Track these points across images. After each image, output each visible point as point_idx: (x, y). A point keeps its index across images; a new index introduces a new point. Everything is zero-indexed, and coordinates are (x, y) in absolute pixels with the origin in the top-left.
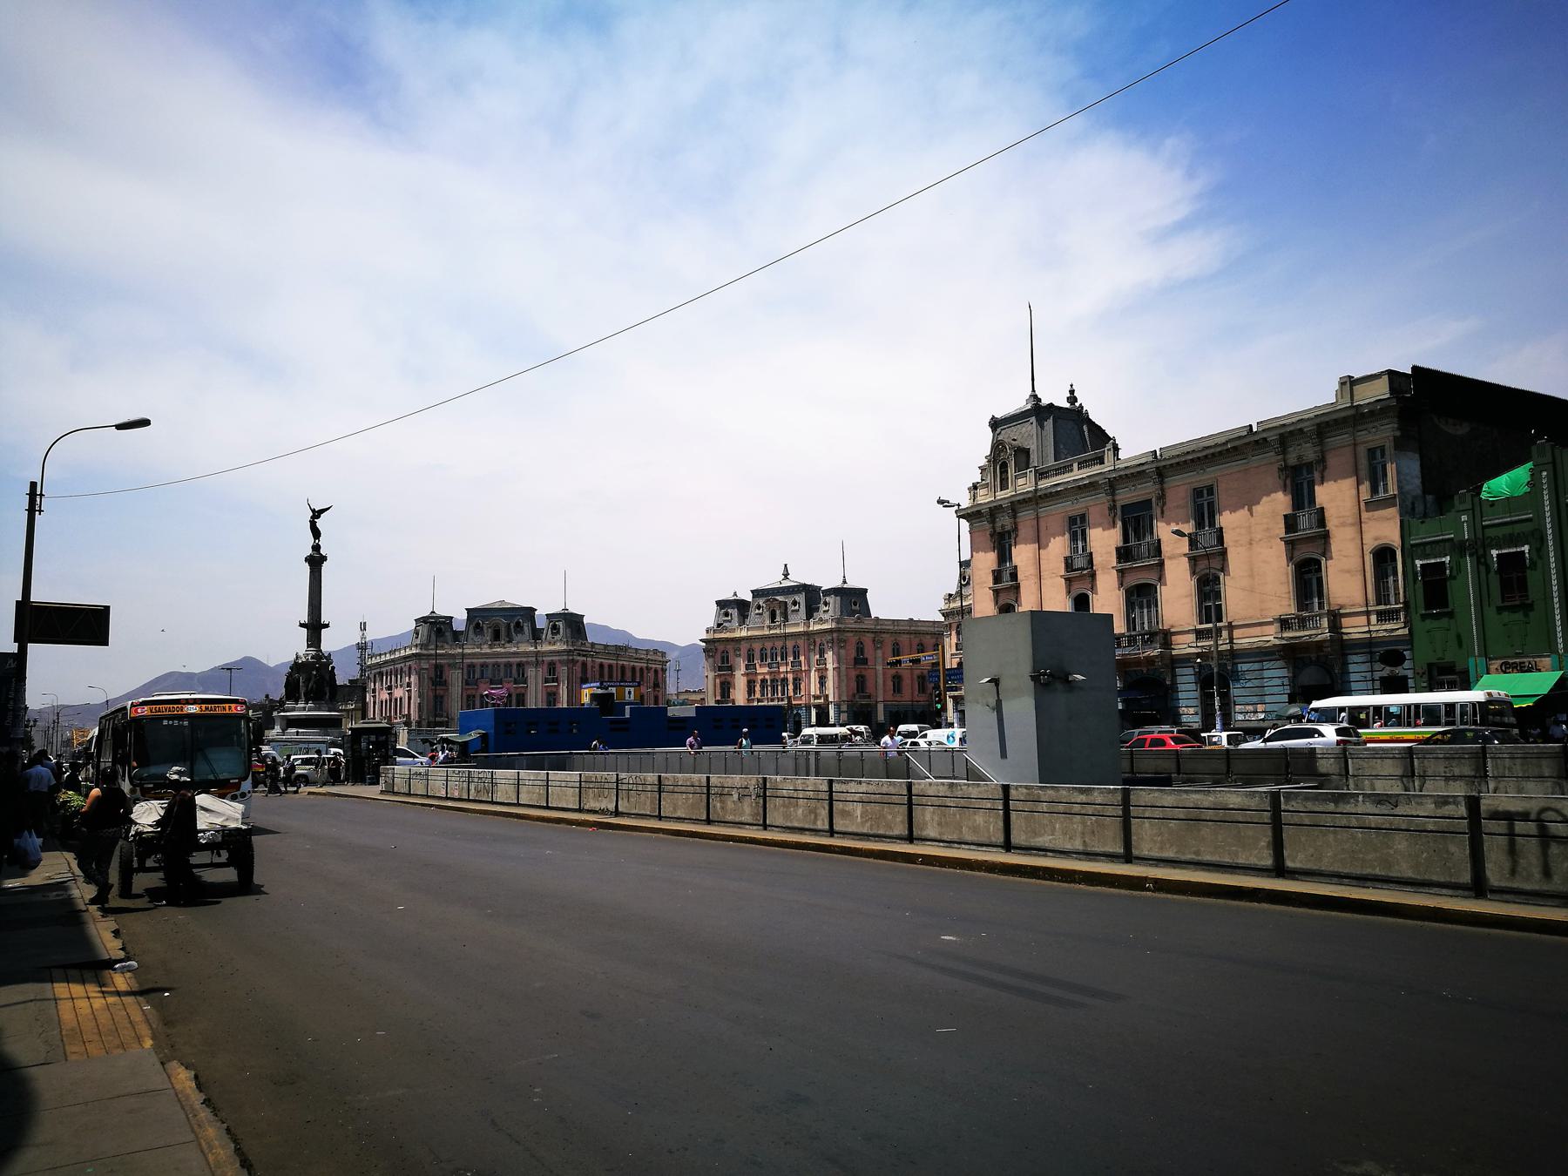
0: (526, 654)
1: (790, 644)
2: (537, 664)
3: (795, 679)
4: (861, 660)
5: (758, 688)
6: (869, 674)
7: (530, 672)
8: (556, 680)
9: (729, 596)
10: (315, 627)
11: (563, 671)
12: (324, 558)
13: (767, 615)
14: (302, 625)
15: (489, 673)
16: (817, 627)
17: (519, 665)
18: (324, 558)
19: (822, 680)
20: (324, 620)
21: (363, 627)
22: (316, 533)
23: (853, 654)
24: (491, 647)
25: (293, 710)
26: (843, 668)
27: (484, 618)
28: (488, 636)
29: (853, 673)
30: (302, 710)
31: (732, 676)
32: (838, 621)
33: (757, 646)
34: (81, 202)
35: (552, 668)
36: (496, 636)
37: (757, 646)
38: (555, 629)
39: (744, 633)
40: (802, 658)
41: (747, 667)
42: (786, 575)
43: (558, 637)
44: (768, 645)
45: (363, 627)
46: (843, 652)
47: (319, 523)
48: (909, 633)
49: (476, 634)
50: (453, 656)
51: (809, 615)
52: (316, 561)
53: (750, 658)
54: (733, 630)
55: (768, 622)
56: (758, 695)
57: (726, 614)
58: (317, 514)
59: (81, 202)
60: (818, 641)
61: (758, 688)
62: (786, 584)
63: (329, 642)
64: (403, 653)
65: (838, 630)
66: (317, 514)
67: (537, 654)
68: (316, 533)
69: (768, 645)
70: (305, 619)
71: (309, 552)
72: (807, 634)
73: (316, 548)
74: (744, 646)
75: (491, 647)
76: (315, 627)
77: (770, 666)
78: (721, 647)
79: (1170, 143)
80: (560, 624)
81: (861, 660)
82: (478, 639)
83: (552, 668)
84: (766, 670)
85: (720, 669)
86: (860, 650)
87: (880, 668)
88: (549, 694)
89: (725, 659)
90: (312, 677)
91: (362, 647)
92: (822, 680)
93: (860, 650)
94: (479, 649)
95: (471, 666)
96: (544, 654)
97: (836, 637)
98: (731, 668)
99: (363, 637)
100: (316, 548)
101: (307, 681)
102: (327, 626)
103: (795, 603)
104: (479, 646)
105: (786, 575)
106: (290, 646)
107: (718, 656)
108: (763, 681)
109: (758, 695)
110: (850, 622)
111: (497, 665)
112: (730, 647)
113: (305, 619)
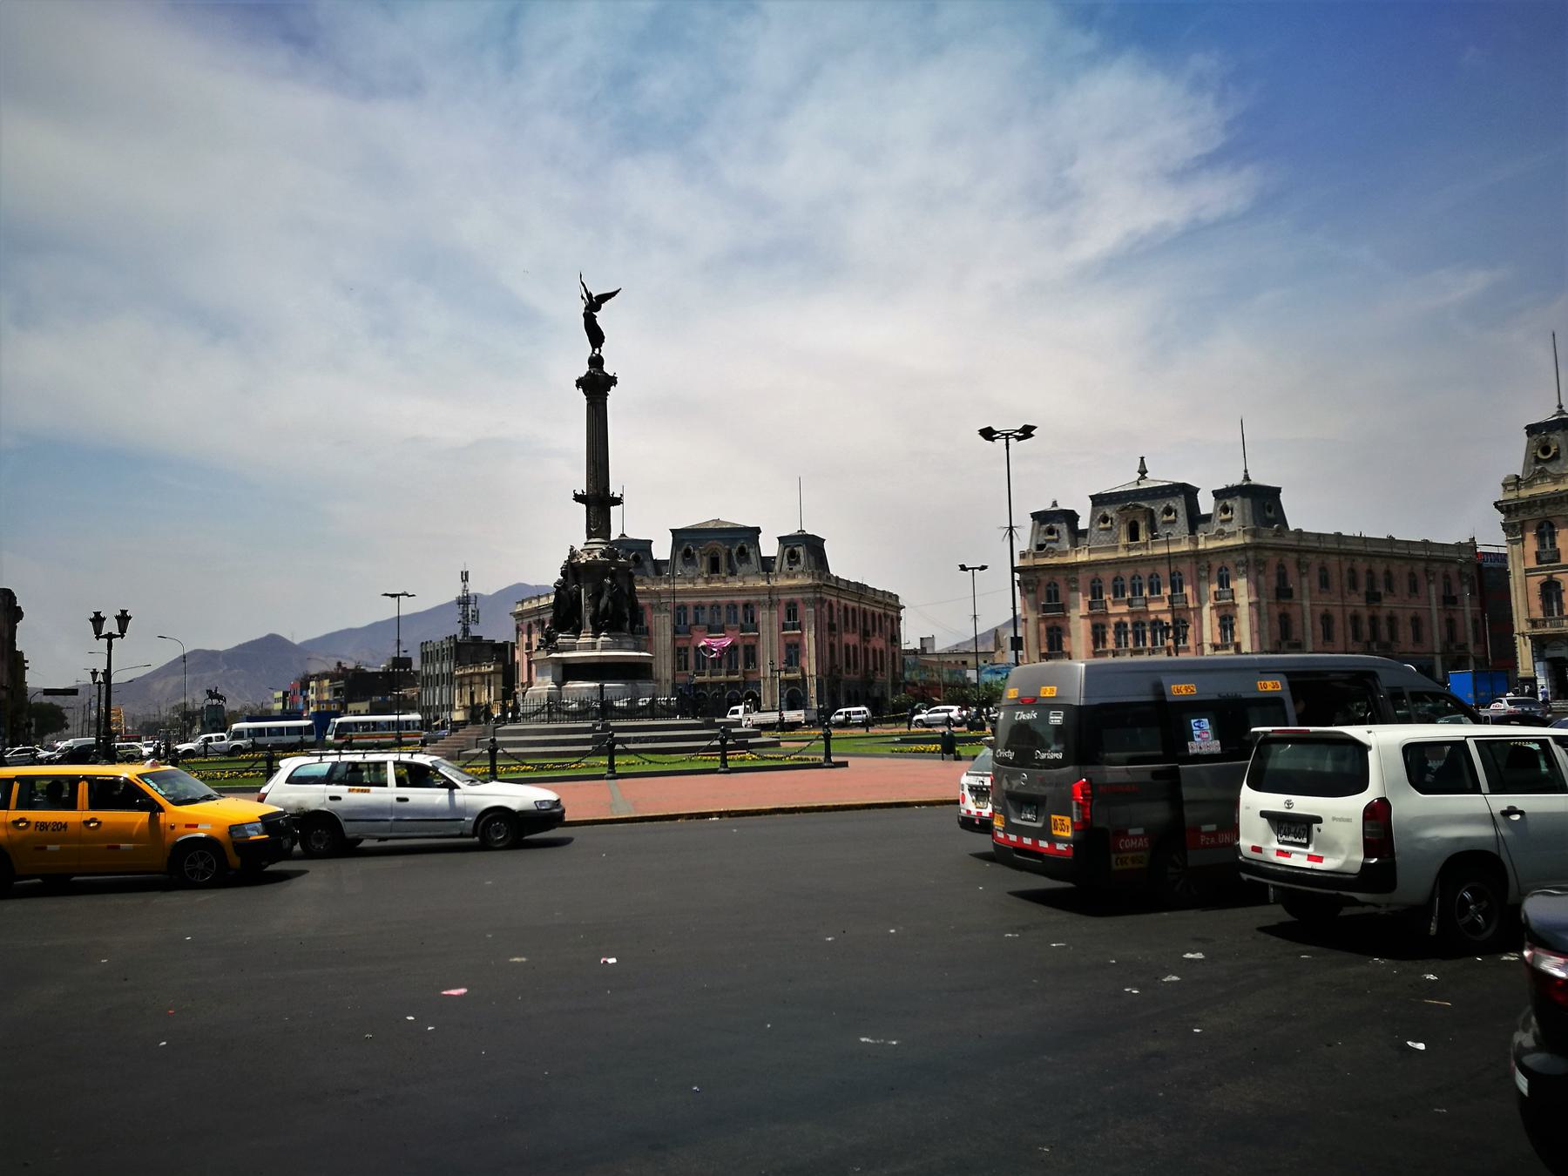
0: (756, 591)
1: (1163, 570)
2: (771, 605)
3: (1135, 625)
4: (1283, 592)
5: (1110, 636)
6: (1294, 612)
7: (762, 616)
8: (799, 626)
9: (1046, 506)
10: (598, 501)
11: (807, 614)
12: (612, 381)
13: (1124, 528)
14: (578, 498)
15: (706, 617)
16: (1211, 545)
17: (746, 606)
18: (612, 381)
19: (1227, 622)
20: (615, 490)
21: (465, 577)
22: (596, 337)
23: (1274, 581)
24: (707, 581)
25: (572, 648)
26: (1264, 602)
27: (697, 542)
28: (704, 568)
29: (1276, 611)
30: (587, 647)
31: (1066, 619)
32: (1254, 534)
33: (1107, 576)
34: (57, 160)
35: (792, 610)
36: (714, 567)
37: (1107, 576)
38: (793, 557)
39: (1082, 557)
40: (1188, 590)
41: (1091, 606)
42: (1143, 472)
43: (797, 568)
44: (1127, 574)
45: (465, 577)
46: (1262, 578)
47: (601, 318)
48: (1340, 553)
49: (685, 563)
50: (658, 594)
51: (1193, 530)
52: (596, 385)
53: (1096, 592)
54: (1065, 553)
55: (1124, 540)
56: (1111, 645)
57: (1051, 531)
58: (594, 304)
59: (57, 160)
60: (1216, 564)
61: (1110, 636)
62: (1144, 485)
63: (623, 524)
64: (535, 604)
65: (1256, 547)
66: (594, 304)
67: (771, 591)
68: (596, 337)
69: (1127, 574)
70: (582, 488)
71: (583, 369)
72: (1197, 555)
73: (596, 362)
74: (1084, 577)
75: (707, 581)
76: (598, 501)
77: (1130, 602)
78: (1045, 578)
79: (1200, 62)
80: (801, 550)
81: (1283, 592)
82: (689, 571)
83: (792, 610)
84: (1124, 609)
85: (1045, 609)
86: (1282, 576)
87: (1307, 603)
88: (789, 646)
89: (1053, 594)
90: (605, 586)
91: (464, 601)
92: (1227, 622)
93: (1282, 576)
94: (694, 585)
95: (683, 607)
96: (779, 590)
97: (1251, 559)
98: (1063, 608)
99: (465, 589)
100: (596, 362)
101: (596, 597)
102: (618, 501)
103: (1168, 511)
104: (692, 580)
105: (1143, 472)
106: (541, 546)
107: (1043, 591)
108: (1120, 627)
109: (1111, 645)
110: (1268, 536)
111: (716, 607)
112: (1060, 578)
113: (582, 488)
